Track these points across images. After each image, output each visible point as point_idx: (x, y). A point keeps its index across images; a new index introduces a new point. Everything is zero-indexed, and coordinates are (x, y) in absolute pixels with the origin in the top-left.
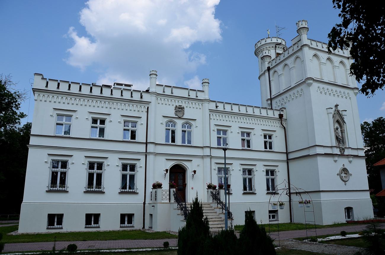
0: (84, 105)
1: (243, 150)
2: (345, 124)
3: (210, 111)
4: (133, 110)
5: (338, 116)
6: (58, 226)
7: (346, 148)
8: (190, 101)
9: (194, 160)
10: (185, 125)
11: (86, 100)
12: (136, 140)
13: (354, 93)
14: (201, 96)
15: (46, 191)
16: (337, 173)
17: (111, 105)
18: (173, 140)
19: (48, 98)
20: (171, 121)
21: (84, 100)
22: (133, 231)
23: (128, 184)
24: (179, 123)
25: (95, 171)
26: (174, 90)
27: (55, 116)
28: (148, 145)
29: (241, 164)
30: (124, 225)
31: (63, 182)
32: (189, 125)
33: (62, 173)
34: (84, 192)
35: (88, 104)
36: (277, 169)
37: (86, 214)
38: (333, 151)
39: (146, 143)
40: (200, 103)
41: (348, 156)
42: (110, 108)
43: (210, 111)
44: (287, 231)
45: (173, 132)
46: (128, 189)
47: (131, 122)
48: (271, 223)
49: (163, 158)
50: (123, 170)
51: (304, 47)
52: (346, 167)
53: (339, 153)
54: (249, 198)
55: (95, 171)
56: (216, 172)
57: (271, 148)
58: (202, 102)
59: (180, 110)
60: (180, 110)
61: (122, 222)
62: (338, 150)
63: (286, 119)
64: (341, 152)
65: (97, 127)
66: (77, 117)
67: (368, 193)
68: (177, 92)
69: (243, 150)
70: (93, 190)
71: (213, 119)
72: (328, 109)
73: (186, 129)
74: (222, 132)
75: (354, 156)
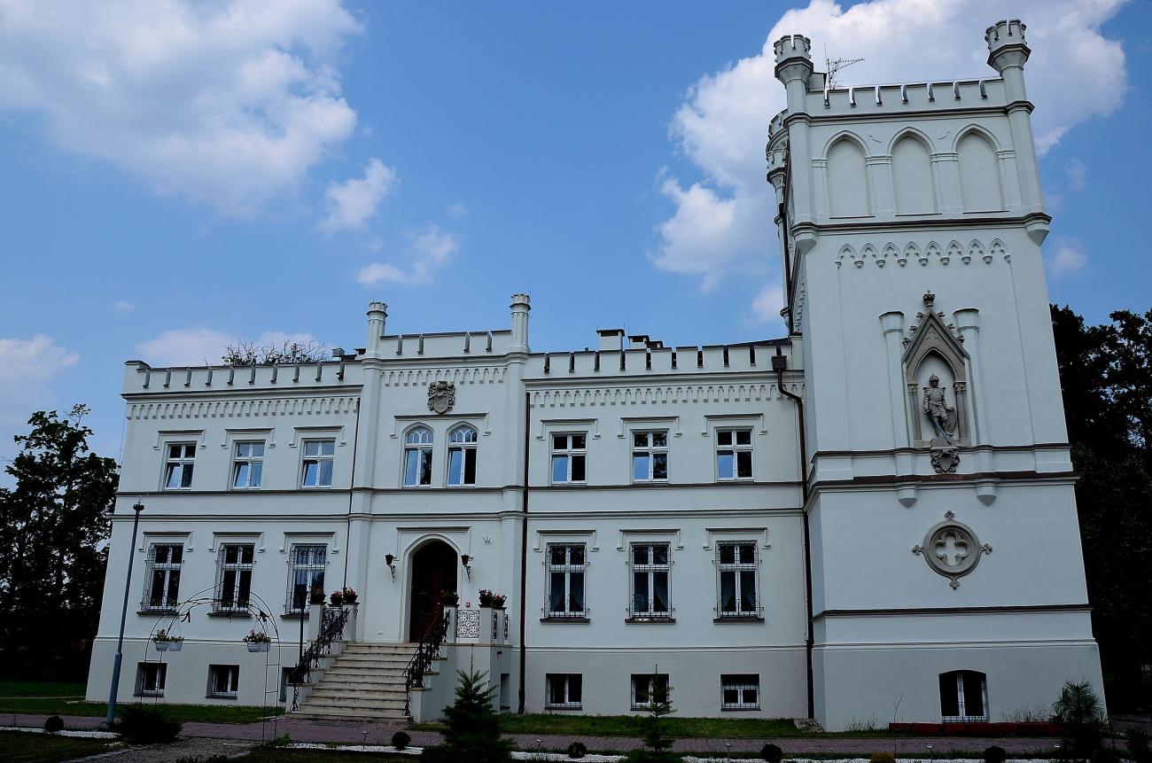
0: (670, 401)
1: (635, 486)
2: (966, 361)
3: (527, 385)
4: (670, 401)
5: (937, 336)
6: (573, 703)
7: (962, 449)
8: (472, 367)
9: (475, 526)
11: (695, 388)
12: (478, 484)
13: (1030, 235)
14: (501, 346)
15: (714, 620)
16: (913, 547)
17: (664, 393)
18: (426, 478)
19: (772, 392)
20: (416, 425)
21: (578, 392)
23: (567, 598)
24: (441, 428)
25: (737, 566)
26: (495, 339)
27: (299, 443)
28: (531, 495)
29: (624, 531)
30: (733, 704)
33: (743, 574)
34: (715, 621)
35: (619, 400)
37: (213, 668)
39: (526, 490)
40: (501, 366)
41: (973, 480)
42: (274, 414)
43: (527, 385)
45: (428, 457)
47: (323, 442)
48: (727, 715)
49: (392, 527)
50: (723, 561)
51: (796, 121)
52: (959, 520)
53: (931, 472)
55: (737, 566)
56: (542, 557)
58: (505, 361)
59: (442, 392)
60: (440, 394)
61: (730, 697)
62: (927, 459)
63: (803, 371)
64: (939, 466)
65: (646, 454)
66: (680, 432)
67: (1085, 619)
68: (434, 349)
69: (635, 486)
70: (736, 614)
71: (537, 406)
72: (884, 319)
73: (464, 442)
74: (181, 450)
75: (1002, 478)
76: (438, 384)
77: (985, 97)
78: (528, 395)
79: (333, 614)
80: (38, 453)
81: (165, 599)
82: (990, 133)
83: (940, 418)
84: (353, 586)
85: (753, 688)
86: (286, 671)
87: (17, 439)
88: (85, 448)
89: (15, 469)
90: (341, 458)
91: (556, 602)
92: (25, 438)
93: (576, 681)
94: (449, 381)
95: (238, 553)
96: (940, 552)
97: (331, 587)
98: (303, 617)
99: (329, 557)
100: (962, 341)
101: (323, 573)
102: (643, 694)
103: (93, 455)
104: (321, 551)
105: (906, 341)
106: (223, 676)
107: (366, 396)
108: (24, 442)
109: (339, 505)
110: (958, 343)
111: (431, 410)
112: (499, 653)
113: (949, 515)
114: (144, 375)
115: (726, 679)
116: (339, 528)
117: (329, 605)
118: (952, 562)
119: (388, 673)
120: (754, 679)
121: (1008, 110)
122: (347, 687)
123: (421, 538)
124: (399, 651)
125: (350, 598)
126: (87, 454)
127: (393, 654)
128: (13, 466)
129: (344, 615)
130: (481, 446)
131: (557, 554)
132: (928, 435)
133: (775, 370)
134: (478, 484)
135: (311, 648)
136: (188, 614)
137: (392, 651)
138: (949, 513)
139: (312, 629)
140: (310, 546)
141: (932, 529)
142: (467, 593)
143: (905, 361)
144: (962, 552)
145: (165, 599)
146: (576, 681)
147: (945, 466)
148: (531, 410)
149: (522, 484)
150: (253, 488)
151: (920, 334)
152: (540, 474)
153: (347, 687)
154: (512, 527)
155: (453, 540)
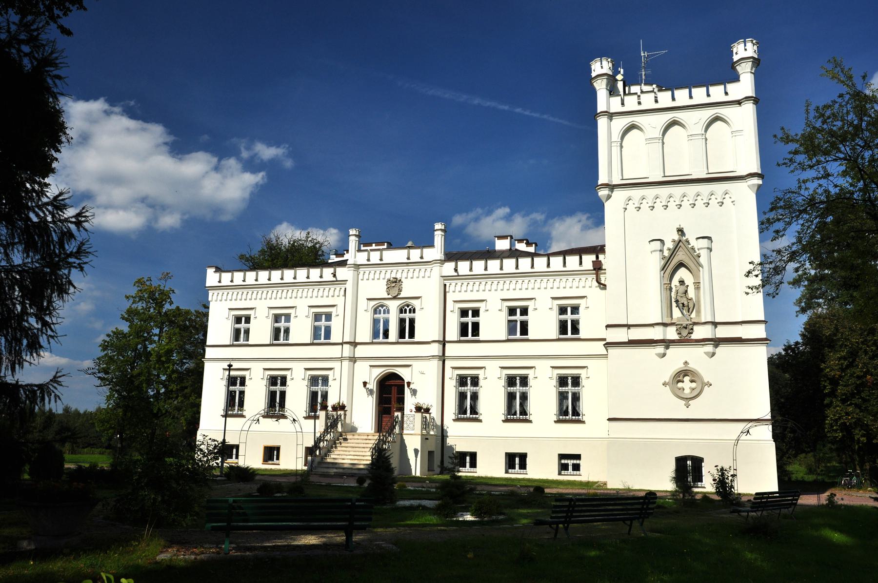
2: (701, 268)
5: (684, 253)
6: (472, 469)
7: (695, 324)
9: (415, 363)
10: (406, 307)
12: (416, 339)
18: (386, 335)
22: (523, 479)
28: (447, 345)
31: (282, 405)
32: (412, 308)
36: (480, 373)
37: (580, 455)
38: (665, 333)
39: (444, 343)
43: (444, 280)
44: (267, 475)
46: (518, 415)
48: (561, 478)
51: (601, 117)
52: (692, 366)
53: (676, 337)
54: (517, 429)
55: (570, 389)
56: (454, 383)
57: (412, 335)
59: (394, 284)
60: (394, 285)
61: (563, 467)
64: (680, 334)
76: (392, 279)
77: (726, 93)
78: (445, 285)
79: (333, 416)
80: (140, 306)
81: (236, 408)
82: (727, 117)
83: (683, 304)
84: (344, 401)
85: (578, 462)
86: (307, 449)
87: (127, 297)
88: (171, 303)
89: (126, 316)
90: (336, 325)
91: (462, 410)
92: (132, 297)
93: (523, 457)
94: (399, 277)
95: (277, 381)
96: (680, 385)
97: (332, 401)
98: (316, 417)
99: (330, 382)
100: (699, 257)
101: (327, 392)
102: (28, 411)
103: (178, 307)
104: (325, 380)
105: (664, 258)
106: (271, 453)
107: (349, 286)
108: (131, 301)
109: (335, 351)
110: (696, 258)
111: (389, 295)
112: (427, 439)
113: (686, 363)
114: (218, 274)
115: (562, 457)
116: (336, 365)
117: (331, 411)
118: (687, 391)
119: (363, 450)
120: (578, 457)
121: (741, 103)
122: (340, 457)
123: (403, 303)
124: (370, 437)
125: (343, 407)
126: (174, 307)
127: (366, 439)
128: (124, 314)
129: (339, 417)
130: (418, 316)
131: (462, 381)
132: (677, 313)
133: (594, 269)
134: (416, 339)
135: (320, 436)
136: (258, 420)
137: (366, 437)
138: (686, 362)
139: (321, 425)
140: (320, 376)
141: (674, 372)
142: (410, 402)
143: (663, 269)
144: (694, 385)
145: (236, 408)
146: (523, 457)
147: (685, 333)
148: (447, 294)
149: (442, 339)
150: (285, 342)
151: (673, 252)
152: (453, 333)
153: (340, 457)
154: (435, 364)
155: (400, 371)
